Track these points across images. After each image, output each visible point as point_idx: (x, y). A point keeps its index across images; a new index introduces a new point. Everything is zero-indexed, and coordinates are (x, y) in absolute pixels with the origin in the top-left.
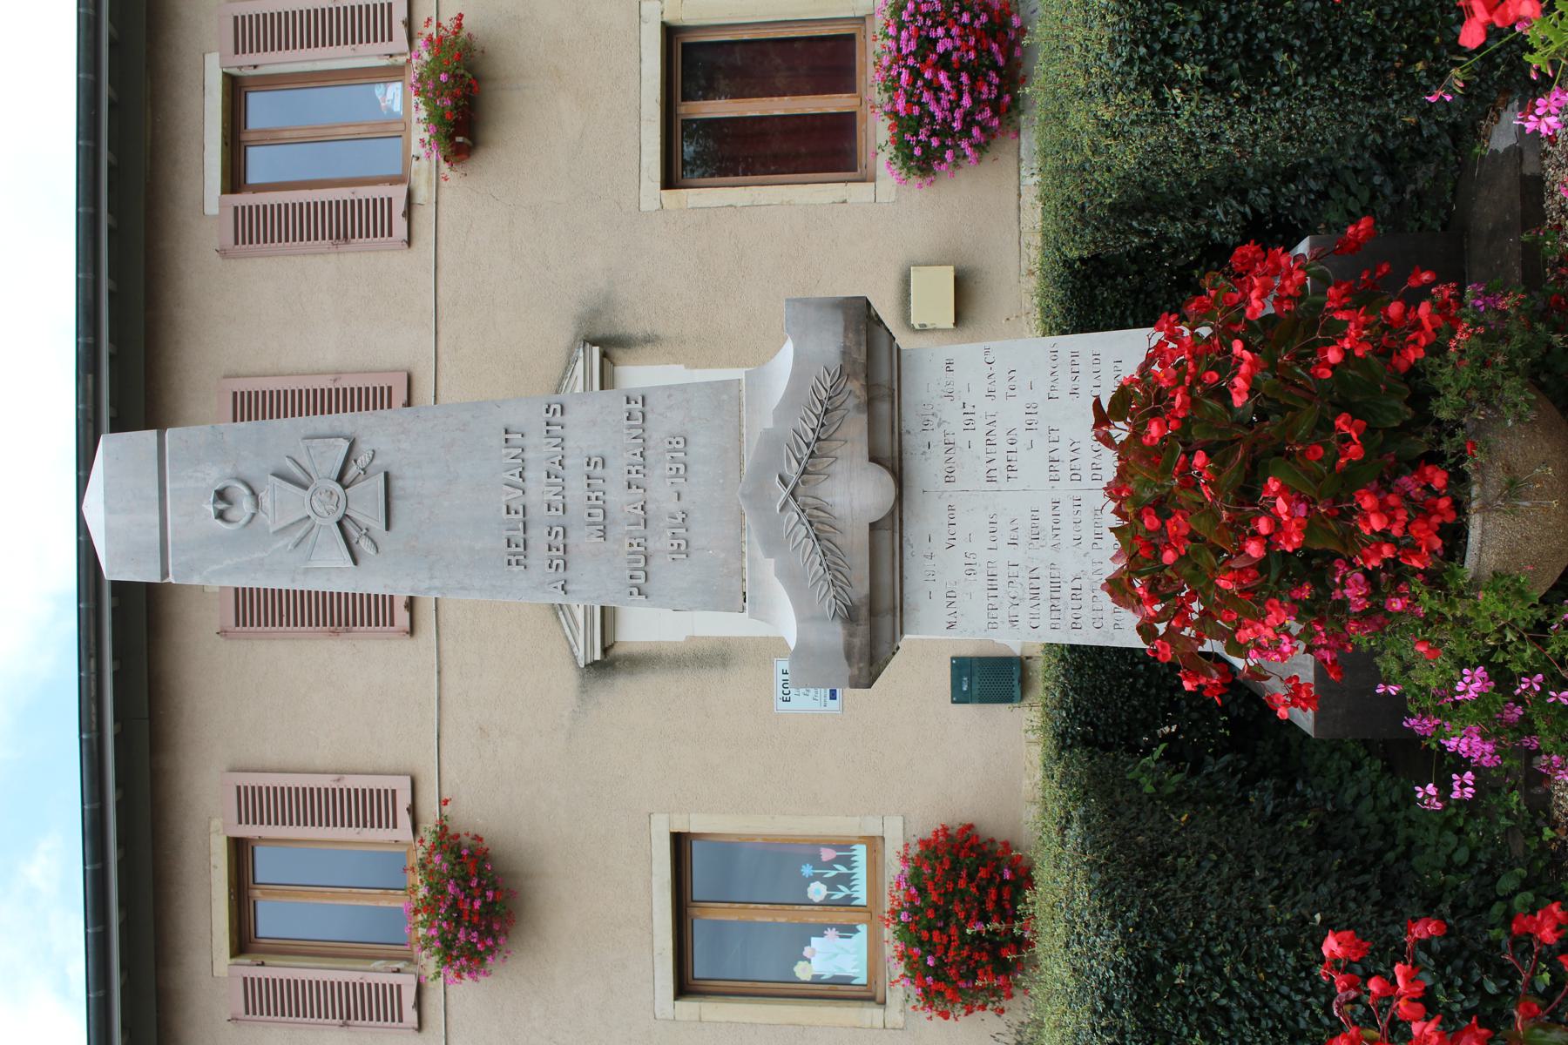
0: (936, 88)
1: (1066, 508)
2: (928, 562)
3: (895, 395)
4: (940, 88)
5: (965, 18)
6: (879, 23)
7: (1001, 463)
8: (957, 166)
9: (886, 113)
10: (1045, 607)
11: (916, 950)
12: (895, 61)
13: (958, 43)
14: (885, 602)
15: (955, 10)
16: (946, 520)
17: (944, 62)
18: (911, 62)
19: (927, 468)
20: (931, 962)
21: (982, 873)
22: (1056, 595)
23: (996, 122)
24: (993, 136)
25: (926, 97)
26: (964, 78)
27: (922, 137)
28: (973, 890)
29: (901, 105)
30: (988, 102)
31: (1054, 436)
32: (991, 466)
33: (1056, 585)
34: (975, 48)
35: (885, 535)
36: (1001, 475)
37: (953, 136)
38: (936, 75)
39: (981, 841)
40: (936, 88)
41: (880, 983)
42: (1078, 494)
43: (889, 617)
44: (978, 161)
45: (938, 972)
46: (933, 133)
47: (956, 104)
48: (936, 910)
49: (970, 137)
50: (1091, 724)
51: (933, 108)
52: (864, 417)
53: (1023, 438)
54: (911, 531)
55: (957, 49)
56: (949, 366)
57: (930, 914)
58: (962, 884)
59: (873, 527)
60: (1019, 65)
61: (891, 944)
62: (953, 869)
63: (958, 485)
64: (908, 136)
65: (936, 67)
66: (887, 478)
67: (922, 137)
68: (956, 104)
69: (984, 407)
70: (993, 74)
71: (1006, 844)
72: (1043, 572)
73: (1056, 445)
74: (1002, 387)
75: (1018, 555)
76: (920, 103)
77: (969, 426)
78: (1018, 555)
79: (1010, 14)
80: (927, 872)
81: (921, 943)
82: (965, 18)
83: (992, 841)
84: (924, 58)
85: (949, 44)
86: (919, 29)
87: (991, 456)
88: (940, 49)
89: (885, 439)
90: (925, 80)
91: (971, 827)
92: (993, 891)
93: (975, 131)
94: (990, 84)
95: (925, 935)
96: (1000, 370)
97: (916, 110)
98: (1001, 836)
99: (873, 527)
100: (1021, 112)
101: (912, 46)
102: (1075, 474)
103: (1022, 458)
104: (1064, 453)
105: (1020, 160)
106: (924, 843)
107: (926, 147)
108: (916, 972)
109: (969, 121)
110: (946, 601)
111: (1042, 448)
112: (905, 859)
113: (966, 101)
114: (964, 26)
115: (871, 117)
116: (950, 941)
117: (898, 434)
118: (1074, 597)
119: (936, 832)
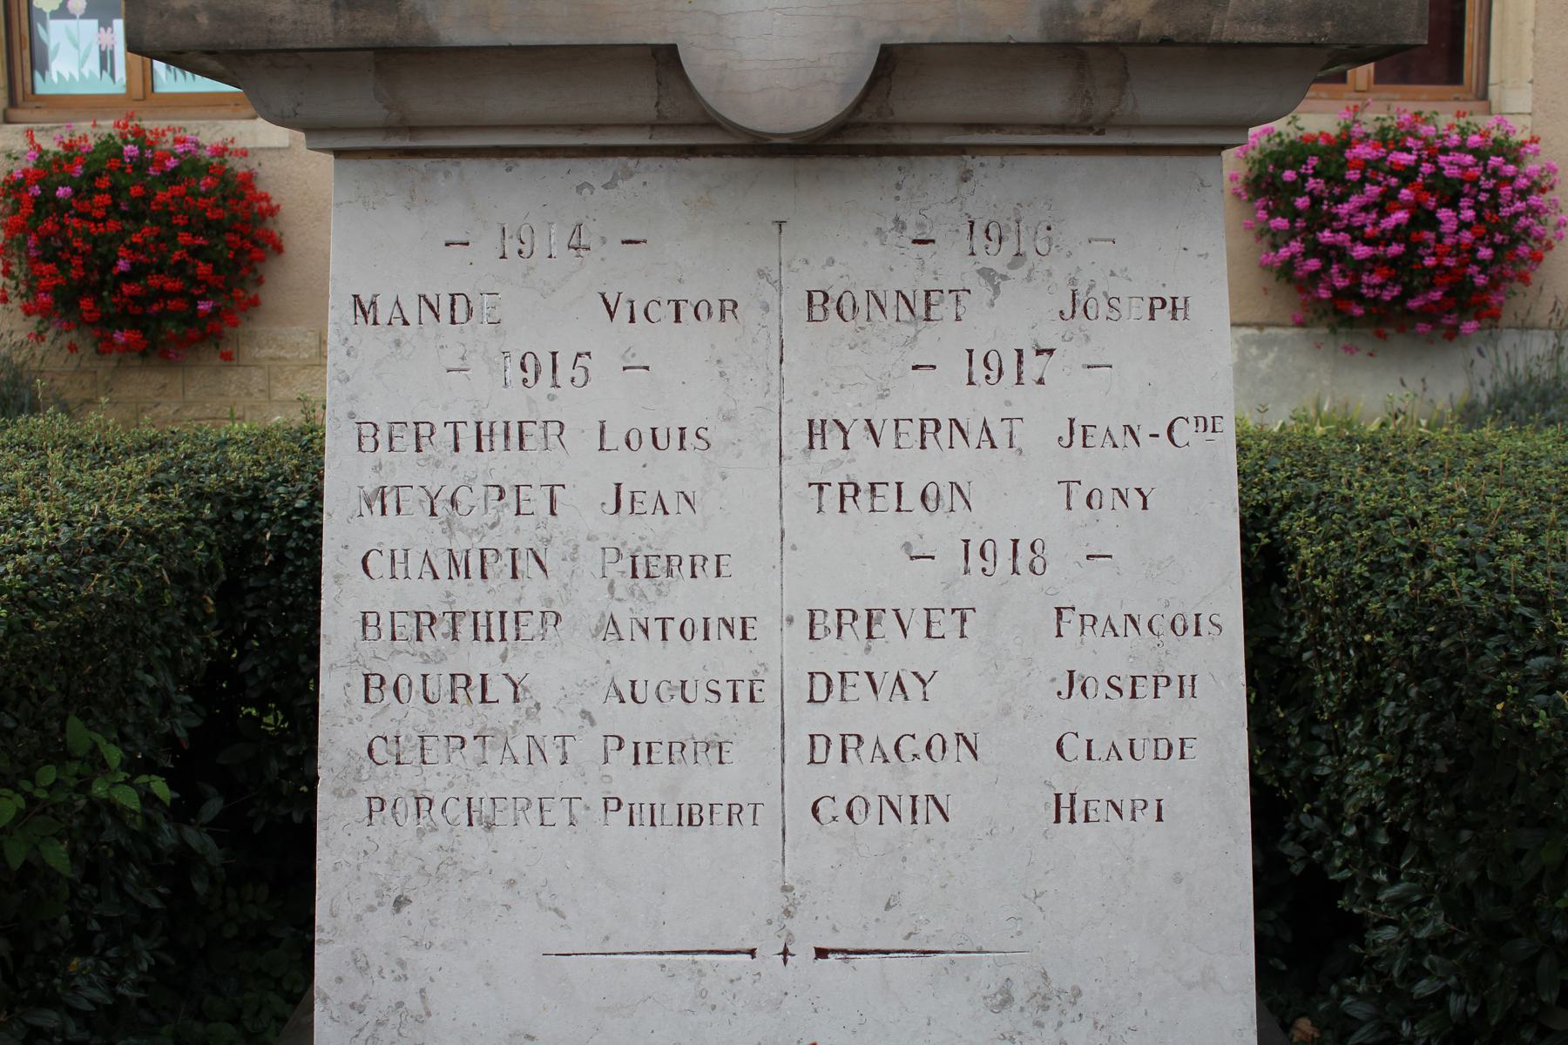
0: (1382, 207)
1: (727, 659)
2: (559, 237)
3: (1085, 137)
4: (1384, 213)
5: (1485, 253)
6: (1484, 122)
7: (865, 462)
8: (1260, 236)
9: (1347, 128)
10: (427, 595)
11: (79, 170)
12: (1428, 146)
13: (1448, 241)
14: (426, 99)
15: (1498, 238)
16: (691, 293)
17: (1423, 218)
18: (1426, 168)
19: (853, 236)
20: (61, 192)
21: (203, 269)
22: (465, 627)
23: (1324, 294)
24: (1301, 289)
25: (1372, 190)
26: (1395, 249)
27: (1311, 183)
28: (177, 255)
29: (1364, 152)
30: (1357, 282)
31: (946, 624)
32: (858, 434)
33: (487, 628)
34: (1439, 266)
35: (640, 99)
36: (829, 462)
37: (1308, 229)
38: (1404, 206)
39: (257, 265)
40: (1382, 207)
41: (37, 114)
42: (768, 694)
43: (375, 112)
44: (1264, 266)
45: (45, 204)
46: (1316, 200)
47: (1357, 234)
48: (143, 198)
49: (1305, 255)
50: (280, 560)
51: (1355, 200)
52: (1031, 31)
53: (941, 531)
54: (655, 190)
55: (1439, 239)
56: (1165, 306)
57: (135, 191)
58: (184, 238)
59: (665, 59)
60: (1401, 329)
61: (91, 131)
62: (208, 225)
63: (800, 334)
64: (1314, 161)
65: (1415, 207)
66: (824, 108)
67: (1311, 183)
68: (1357, 234)
69: (1039, 413)
70: (1396, 291)
71: (255, 302)
72: (533, 591)
73: (917, 629)
74: (1100, 467)
75: (584, 513)
76: (1363, 180)
77: (984, 367)
78: (584, 513)
79: (1478, 317)
80: (204, 184)
81: (92, 177)
82: (1485, 253)
83: (260, 281)
84: (1430, 189)
85: (1449, 226)
86: (1475, 182)
87: (887, 436)
88: (1443, 214)
89: (945, 100)
90: (1397, 189)
91: (279, 249)
92: (178, 285)
93: (1313, 264)
94: (1382, 287)
95: (104, 183)
96: (1151, 462)
97: (1353, 175)
98: (267, 294)
99: (665, 59)
100: (1333, 331)
101: (1451, 172)
102: (831, 685)
103: (884, 530)
104: (894, 653)
105: (1260, 326)
106: (248, 180)
107: (1296, 188)
108: (47, 170)
109: (1331, 254)
110: (439, 290)
111: (912, 589)
112: (220, 151)
113: (1361, 251)
114: (1473, 250)
115: (1340, 106)
116: (96, 221)
117: (960, 144)
118: (460, 682)
119: (267, 198)
